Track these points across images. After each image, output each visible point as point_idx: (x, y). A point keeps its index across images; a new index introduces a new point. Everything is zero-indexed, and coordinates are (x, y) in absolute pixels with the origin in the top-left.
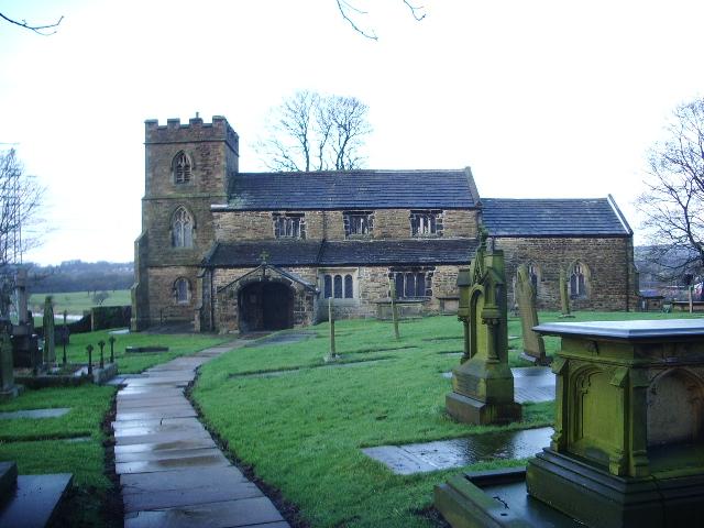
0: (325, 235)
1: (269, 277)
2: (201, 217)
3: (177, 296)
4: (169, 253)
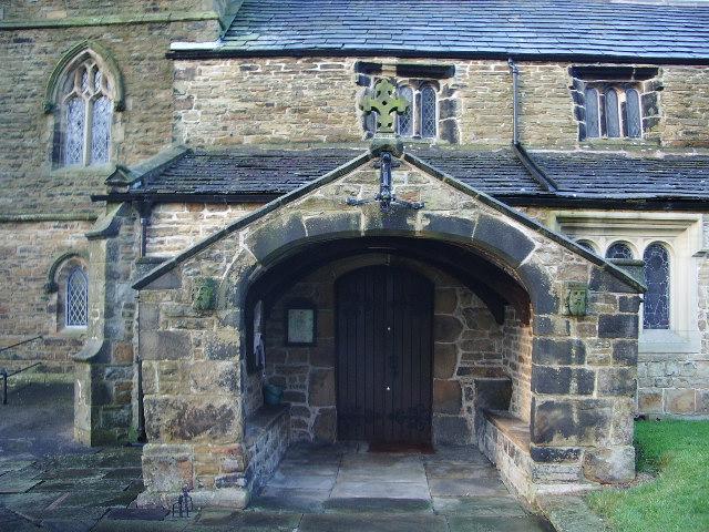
0: (518, 131)
1: (410, 209)
2: (139, 77)
3: (59, 309)
4: (40, 184)
